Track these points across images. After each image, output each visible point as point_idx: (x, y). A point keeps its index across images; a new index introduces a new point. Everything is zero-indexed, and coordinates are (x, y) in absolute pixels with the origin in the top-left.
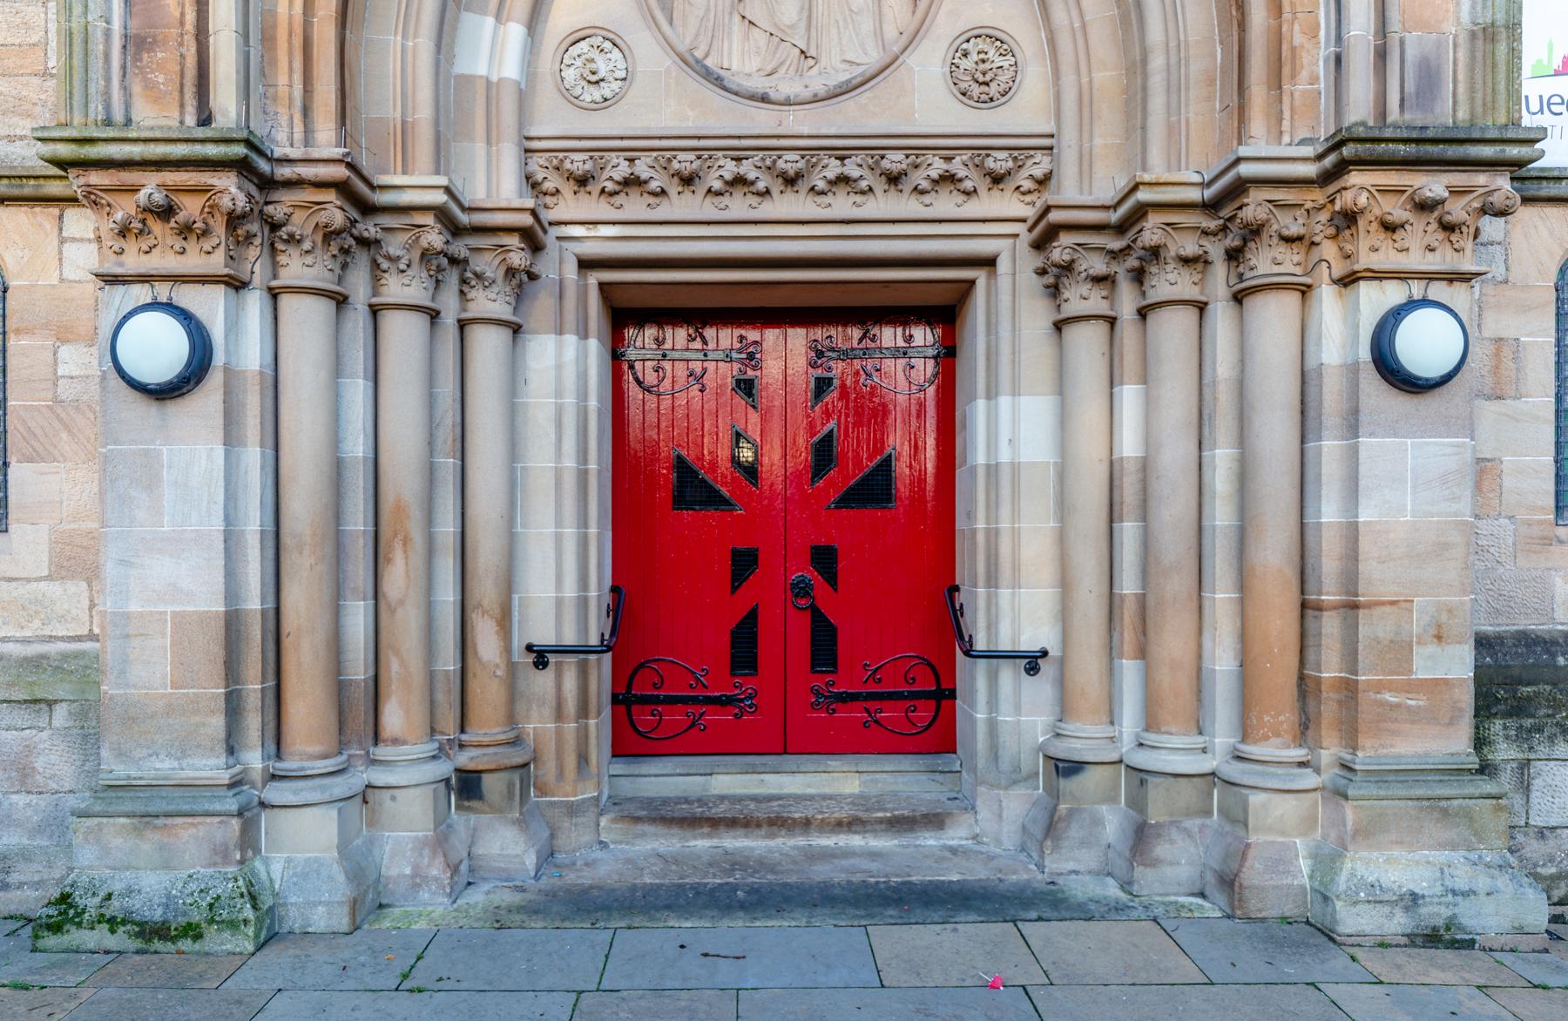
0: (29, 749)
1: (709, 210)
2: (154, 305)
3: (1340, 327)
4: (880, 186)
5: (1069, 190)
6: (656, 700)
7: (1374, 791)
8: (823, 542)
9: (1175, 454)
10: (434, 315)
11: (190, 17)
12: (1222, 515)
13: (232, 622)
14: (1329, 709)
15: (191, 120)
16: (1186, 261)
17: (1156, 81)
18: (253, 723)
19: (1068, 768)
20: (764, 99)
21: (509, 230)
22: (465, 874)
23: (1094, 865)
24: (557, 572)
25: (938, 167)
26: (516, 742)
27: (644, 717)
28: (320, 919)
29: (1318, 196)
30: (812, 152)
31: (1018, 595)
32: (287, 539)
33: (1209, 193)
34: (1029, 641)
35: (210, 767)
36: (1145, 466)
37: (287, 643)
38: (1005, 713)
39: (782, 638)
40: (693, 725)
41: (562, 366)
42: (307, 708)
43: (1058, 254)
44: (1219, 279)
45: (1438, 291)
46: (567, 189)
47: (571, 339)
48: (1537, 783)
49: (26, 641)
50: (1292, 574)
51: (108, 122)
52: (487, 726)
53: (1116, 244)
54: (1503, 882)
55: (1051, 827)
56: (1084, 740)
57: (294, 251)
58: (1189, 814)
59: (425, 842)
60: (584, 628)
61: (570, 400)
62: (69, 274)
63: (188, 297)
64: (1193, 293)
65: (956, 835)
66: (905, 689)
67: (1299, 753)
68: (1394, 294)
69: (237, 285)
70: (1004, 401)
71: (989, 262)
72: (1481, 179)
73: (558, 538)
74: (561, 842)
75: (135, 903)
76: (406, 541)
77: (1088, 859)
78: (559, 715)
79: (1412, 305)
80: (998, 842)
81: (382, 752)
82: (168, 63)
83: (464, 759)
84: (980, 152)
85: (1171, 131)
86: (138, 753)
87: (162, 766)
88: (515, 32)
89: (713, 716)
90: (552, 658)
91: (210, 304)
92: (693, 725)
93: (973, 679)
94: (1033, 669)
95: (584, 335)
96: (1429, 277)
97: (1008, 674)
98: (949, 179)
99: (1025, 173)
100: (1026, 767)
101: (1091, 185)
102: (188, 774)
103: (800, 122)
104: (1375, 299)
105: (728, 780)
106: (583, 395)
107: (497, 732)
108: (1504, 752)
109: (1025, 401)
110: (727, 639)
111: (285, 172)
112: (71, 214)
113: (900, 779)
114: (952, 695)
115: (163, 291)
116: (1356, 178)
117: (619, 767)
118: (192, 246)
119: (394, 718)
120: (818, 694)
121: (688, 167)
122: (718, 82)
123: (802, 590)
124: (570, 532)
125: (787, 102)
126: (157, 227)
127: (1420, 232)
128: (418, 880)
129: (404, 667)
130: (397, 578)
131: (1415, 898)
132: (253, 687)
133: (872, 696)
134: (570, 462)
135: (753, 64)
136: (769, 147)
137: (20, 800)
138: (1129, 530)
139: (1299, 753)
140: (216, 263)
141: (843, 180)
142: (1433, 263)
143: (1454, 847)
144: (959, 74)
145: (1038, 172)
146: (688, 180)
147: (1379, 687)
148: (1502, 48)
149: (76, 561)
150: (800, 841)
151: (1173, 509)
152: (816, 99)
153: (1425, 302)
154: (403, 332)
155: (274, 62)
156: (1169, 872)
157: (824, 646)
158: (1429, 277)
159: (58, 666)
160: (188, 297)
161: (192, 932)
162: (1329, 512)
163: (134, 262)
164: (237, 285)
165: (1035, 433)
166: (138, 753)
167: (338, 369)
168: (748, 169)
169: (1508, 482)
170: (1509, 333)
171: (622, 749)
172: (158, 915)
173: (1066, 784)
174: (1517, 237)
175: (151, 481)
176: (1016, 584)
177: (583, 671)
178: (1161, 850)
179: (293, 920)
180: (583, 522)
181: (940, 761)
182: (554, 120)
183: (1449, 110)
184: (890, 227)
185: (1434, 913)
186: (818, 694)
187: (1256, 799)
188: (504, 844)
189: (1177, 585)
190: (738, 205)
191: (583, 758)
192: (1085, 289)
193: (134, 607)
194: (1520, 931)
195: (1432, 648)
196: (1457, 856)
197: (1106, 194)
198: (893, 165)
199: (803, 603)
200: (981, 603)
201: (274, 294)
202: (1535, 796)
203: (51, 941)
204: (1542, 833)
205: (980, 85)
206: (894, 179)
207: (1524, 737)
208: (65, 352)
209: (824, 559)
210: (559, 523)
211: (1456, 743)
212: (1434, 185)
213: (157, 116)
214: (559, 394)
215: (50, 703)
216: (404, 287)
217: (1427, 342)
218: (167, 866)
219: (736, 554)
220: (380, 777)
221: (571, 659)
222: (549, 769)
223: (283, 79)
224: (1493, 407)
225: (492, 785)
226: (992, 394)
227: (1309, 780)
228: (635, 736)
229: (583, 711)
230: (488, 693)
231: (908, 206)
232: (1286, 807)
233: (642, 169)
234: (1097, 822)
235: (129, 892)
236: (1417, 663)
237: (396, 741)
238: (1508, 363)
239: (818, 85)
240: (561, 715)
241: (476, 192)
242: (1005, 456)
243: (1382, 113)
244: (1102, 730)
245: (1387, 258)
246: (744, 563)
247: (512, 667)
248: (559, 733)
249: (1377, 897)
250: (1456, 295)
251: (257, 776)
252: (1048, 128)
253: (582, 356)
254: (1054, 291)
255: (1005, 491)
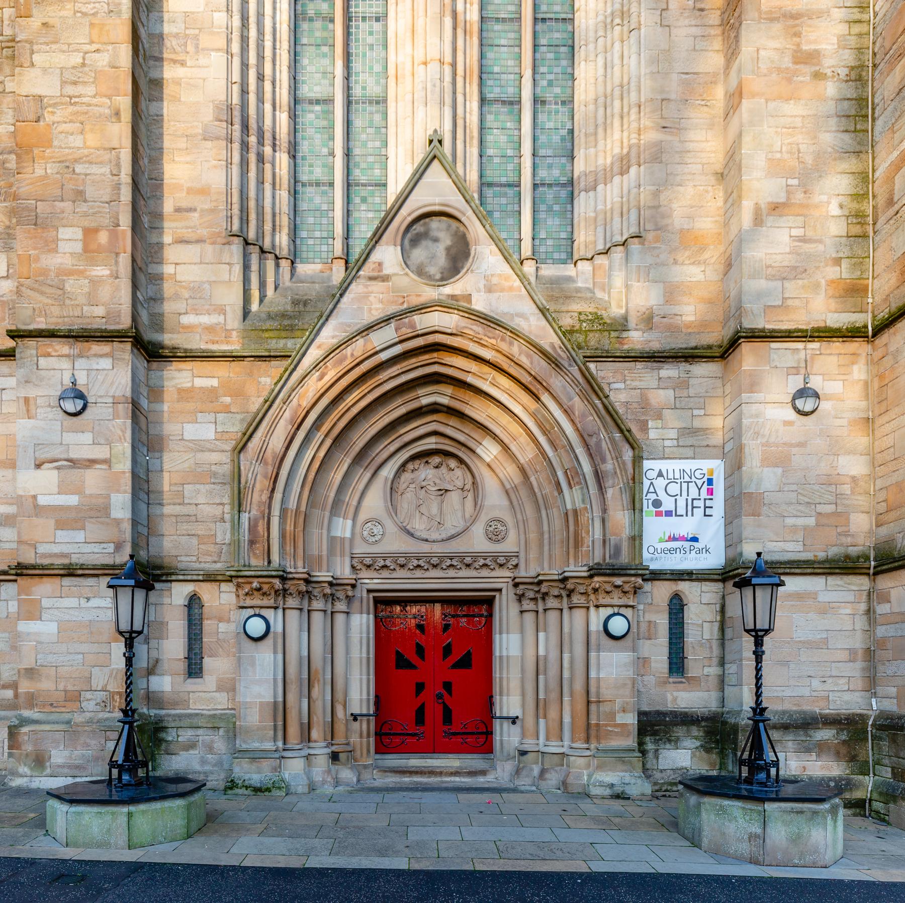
0: (212, 741)
1: (409, 574)
2: (255, 615)
3: (596, 618)
4: (464, 567)
5: (522, 572)
6: (390, 734)
7: (603, 755)
8: (447, 680)
9: (554, 655)
10: (325, 611)
11: (266, 535)
12: (566, 674)
13: (275, 703)
14: (593, 733)
15: (266, 564)
16: (556, 596)
17: (546, 542)
18: (280, 734)
19: (523, 753)
20: (427, 540)
21: (347, 585)
22: (337, 783)
23: (530, 783)
24: (359, 692)
25: (482, 562)
26: (348, 744)
27: (387, 740)
28: (300, 790)
29: (587, 582)
30: (442, 558)
31: (510, 700)
32: (288, 680)
33: (560, 577)
34: (513, 714)
35: (269, 745)
36: (546, 657)
37: (288, 711)
38: (506, 737)
39: (434, 713)
40: (403, 743)
41: (361, 624)
42: (293, 730)
43: (519, 592)
44: (565, 605)
45: (623, 611)
46: (364, 569)
47: (365, 616)
48: (661, 756)
49: (209, 710)
50: (584, 692)
51: (245, 566)
52: (340, 739)
53: (536, 589)
54: (639, 781)
55: (518, 772)
56: (529, 744)
57: (290, 597)
58: (557, 766)
59: (325, 771)
60: (369, 709)
61: (364, 635)
62: (222, 602)
63: (264, 612)
64: (559, 606)
65: (490, 777)
66: (475, 731)
67: (586, 746)
68: (610, 611)
69: (276, 608)
70: (504, 636)
71: (500, 590)
72: (633, 579)
73: (361, 679)
74: (362, 777)
75: (252, 782)
76: (318, 681)
77: (528, 781)
78: (361, 736)
79: (614, 614)
80: (503, 779)
81: (312, 745)
82: (260, 548)
83: (334, 748)
84: (495, 559)
85: (550, 556)
86: (250, 741)
87: (256, 745)
88: (349, 523)
89: (409, 740)
90: (359, 718)
91: (269, 614)
92: (403, 743)
93: (497, 724)
94: (514, 723)
95: (368, 614)
96: (620, 606)
97: (506, 724)
98: (485, 565)
99: (510, 563)
100: (512, 754)
101: (527, 572)
102: (263, 747)
103: (438, 548)
104: (605, 612)
105: (415, 761)
106: (368, 633)
107: (343, 741)
108: (650, 746)
109: (511, 636)
110: (414, 714)
111: (290, 576)
112: (223, 585)
113: (474, 761)
114: (492, 733)
115: (257, 611)
116: (596, 579)
117: (378, 756)
118: (265, 598)
119: (315, 734)
120: (445, 732)
121: (402, 562)
122: (412, 535)
123: (440, 697)
124: (365, 677)
125: (434, 541)
126: (255, 593)
127: (616, 594)
128: (324, 782)
129: (318, 718)
130: (315, 692)
131: (612, 785)
132: (280, 723)
133: (463, 733)
134: (364, 655)
135: (423, 527)
136: (428, 557)
137: (210, 756)
138: (541, 677)
139: (586, 746)
140: (271, 602)
141: (452, 566)
142: (621, 602)
143: (626, 772)
144: (488, 532)
145: (514, 563)
146: (402, 566)
147: (606, 725)
148: (637, 542)
149: (229, 687)
150: (439, 779)
151: (553, 671)
152: (443, 540)
153: (618, 614)
154: (317, 617)
155: (285, 543)
156: (549, 782)
157: (447, 716)
158: (620, 606)
159: (221, 717)
160: (264, 612)
161: (268, 790)
162: (593, 674)
163: (249, 602)
164: (276, 608)
165: (514, 644)
166: (250, 741)
167: (301, 630)
168: (421, 563)
169: (653, 665)
170: (653, 619)
171: (377, 752)
172: (259, 785)
173: (525, 758)
174: (655, 591)
175: (253, 664)
176: (508, 695)
177: (368, 721)
178: (548, 776)
179: (293, 790)
180: (368, 674)
181: (487, 756)
182: (360, 549)
183: (624, 558)
184: (467, 581)
185: (618, 789)
186: (445, 732)
187: (572, 758)
188: (347, 774)
189: (554, 695)
190: (418, 573)
191: (368, 751)
192: (528, 601)
193: (248, 700)
194: (643, 795)
195: (622, 714)
196: (627, 774)
197: (533, 574)
198: (468, 561)
199: (440, 701)
200: (498, 701)
201: (284, 609)
202: (660, 760)
203: (230, 792)
204: (661, 771)
205: (495, 536)
206: (468, 566)
207: (656, 742)
208: (221, 625)
209: (448, 686)
210: (361, 675)
211: (631, 742)
212: (618, 581)
213: (257, 562)
214: (361, 633)
215: (218, 728)
216: (318, 604)
217: (618, 625)
218: (259, 773)
219: (417, 684)
220: (312, 752)
221: (365, 718)
222: (358, 753)
223: (288, 548)
224: (648, 642)
225: (342, 756)
226: (501, 633)
227: (588, 753)
228: (382, 748)
229: (368, 736)
230: (340, 728)
231: (474, 573)
232: (581, 761)
233: (388, 563)
234: (532, 770)
235: (250, 779)
236: (617, 718)
237: (315, 741)
238: (652, 629)
239: (444, 536)
240: (360, 736)
241: (338, 574)
242: (505, 653)
243: (604, 559)
244: (535, 741)
245: (607, 600)
246: (420, 687)
247: (347, 720)
248: (361, 743)
249: (602, 785)
250: (628, 612)
251: (281, 750)
252: (516, 550)
253: (368, 619)
254: (520, 601)
255: (505, 665)
